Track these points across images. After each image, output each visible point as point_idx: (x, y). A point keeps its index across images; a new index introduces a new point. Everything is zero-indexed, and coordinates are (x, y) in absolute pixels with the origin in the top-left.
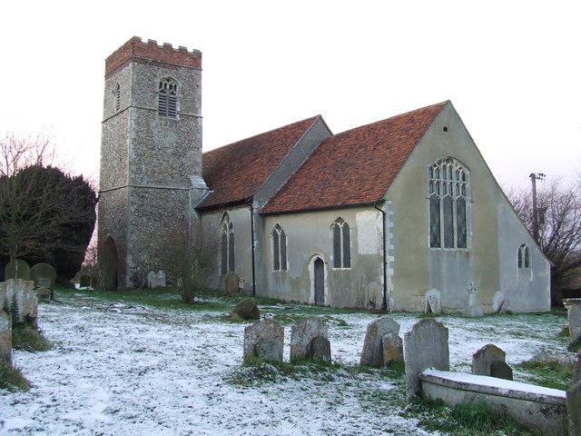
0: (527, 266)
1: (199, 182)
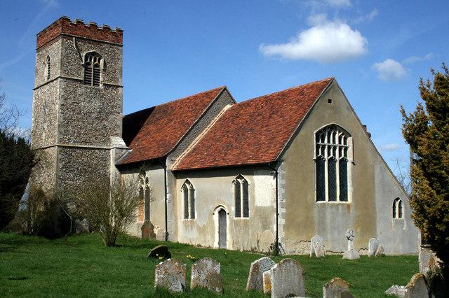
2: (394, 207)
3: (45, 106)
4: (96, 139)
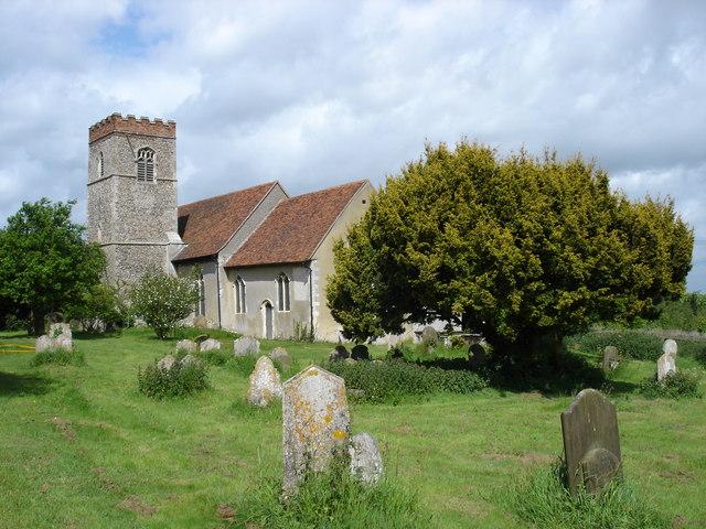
1: (175, 237)
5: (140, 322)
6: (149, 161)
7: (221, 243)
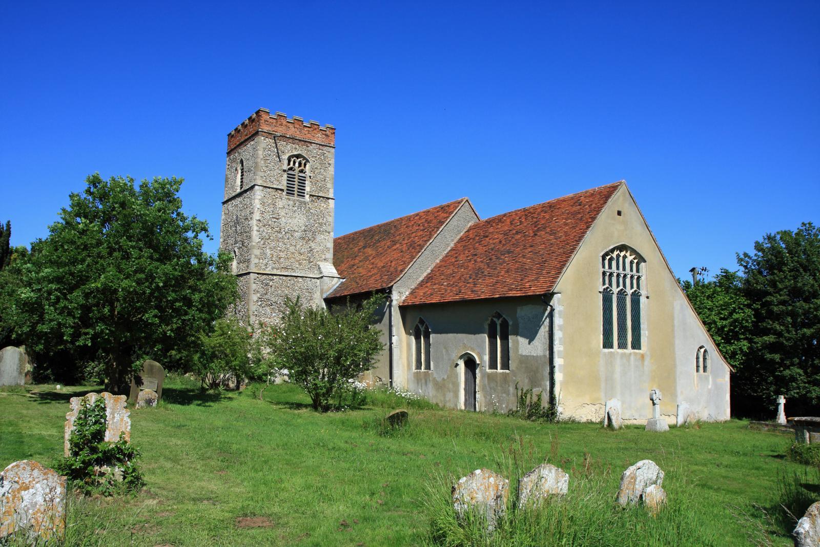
0: (705, 370)
1: (329, 269)
2: (698, 358)
3: (237, 222)
4: (300, 264)
5: (282, 376)
6: (301, 171)
7: (395, 274)
